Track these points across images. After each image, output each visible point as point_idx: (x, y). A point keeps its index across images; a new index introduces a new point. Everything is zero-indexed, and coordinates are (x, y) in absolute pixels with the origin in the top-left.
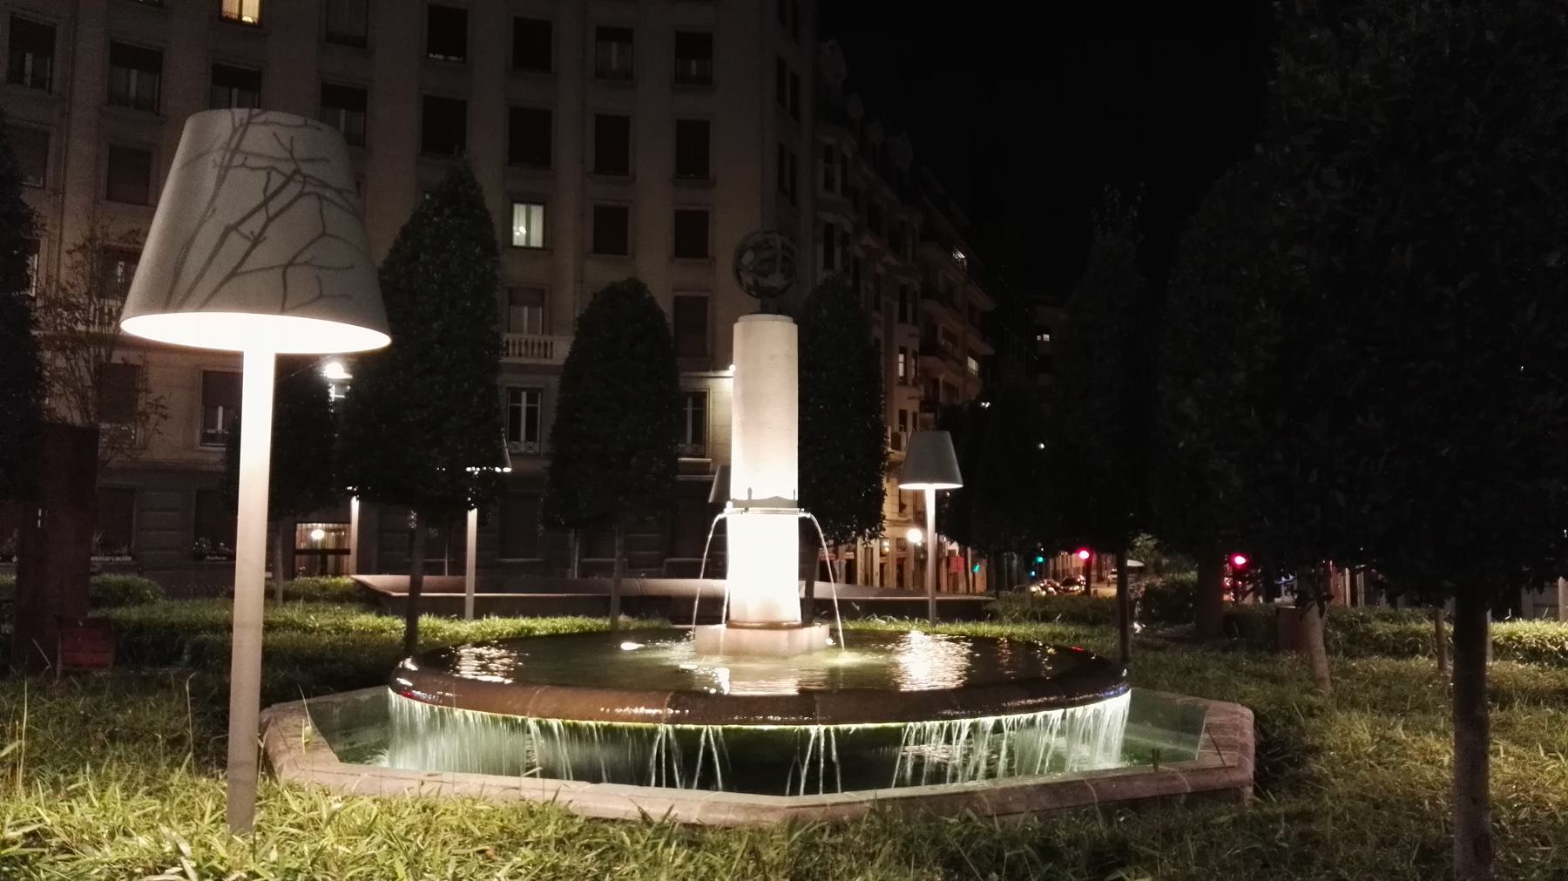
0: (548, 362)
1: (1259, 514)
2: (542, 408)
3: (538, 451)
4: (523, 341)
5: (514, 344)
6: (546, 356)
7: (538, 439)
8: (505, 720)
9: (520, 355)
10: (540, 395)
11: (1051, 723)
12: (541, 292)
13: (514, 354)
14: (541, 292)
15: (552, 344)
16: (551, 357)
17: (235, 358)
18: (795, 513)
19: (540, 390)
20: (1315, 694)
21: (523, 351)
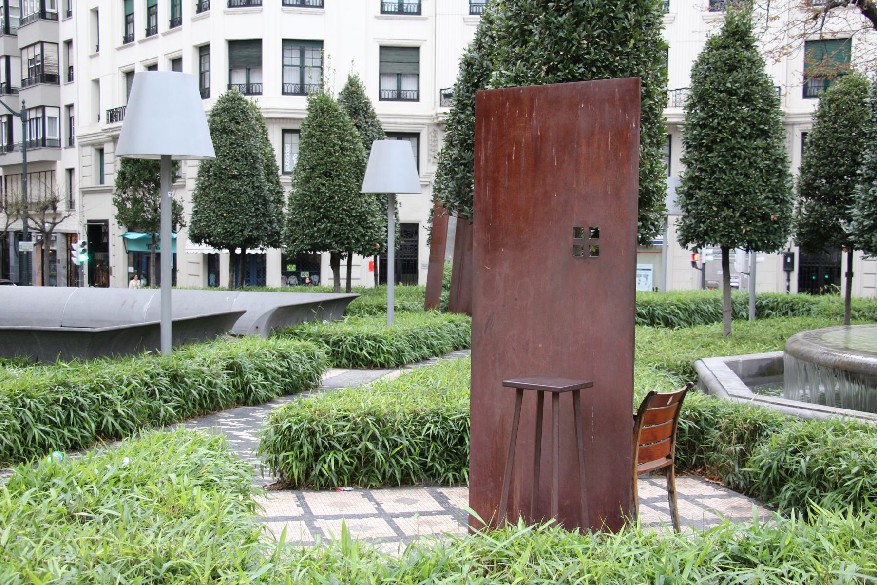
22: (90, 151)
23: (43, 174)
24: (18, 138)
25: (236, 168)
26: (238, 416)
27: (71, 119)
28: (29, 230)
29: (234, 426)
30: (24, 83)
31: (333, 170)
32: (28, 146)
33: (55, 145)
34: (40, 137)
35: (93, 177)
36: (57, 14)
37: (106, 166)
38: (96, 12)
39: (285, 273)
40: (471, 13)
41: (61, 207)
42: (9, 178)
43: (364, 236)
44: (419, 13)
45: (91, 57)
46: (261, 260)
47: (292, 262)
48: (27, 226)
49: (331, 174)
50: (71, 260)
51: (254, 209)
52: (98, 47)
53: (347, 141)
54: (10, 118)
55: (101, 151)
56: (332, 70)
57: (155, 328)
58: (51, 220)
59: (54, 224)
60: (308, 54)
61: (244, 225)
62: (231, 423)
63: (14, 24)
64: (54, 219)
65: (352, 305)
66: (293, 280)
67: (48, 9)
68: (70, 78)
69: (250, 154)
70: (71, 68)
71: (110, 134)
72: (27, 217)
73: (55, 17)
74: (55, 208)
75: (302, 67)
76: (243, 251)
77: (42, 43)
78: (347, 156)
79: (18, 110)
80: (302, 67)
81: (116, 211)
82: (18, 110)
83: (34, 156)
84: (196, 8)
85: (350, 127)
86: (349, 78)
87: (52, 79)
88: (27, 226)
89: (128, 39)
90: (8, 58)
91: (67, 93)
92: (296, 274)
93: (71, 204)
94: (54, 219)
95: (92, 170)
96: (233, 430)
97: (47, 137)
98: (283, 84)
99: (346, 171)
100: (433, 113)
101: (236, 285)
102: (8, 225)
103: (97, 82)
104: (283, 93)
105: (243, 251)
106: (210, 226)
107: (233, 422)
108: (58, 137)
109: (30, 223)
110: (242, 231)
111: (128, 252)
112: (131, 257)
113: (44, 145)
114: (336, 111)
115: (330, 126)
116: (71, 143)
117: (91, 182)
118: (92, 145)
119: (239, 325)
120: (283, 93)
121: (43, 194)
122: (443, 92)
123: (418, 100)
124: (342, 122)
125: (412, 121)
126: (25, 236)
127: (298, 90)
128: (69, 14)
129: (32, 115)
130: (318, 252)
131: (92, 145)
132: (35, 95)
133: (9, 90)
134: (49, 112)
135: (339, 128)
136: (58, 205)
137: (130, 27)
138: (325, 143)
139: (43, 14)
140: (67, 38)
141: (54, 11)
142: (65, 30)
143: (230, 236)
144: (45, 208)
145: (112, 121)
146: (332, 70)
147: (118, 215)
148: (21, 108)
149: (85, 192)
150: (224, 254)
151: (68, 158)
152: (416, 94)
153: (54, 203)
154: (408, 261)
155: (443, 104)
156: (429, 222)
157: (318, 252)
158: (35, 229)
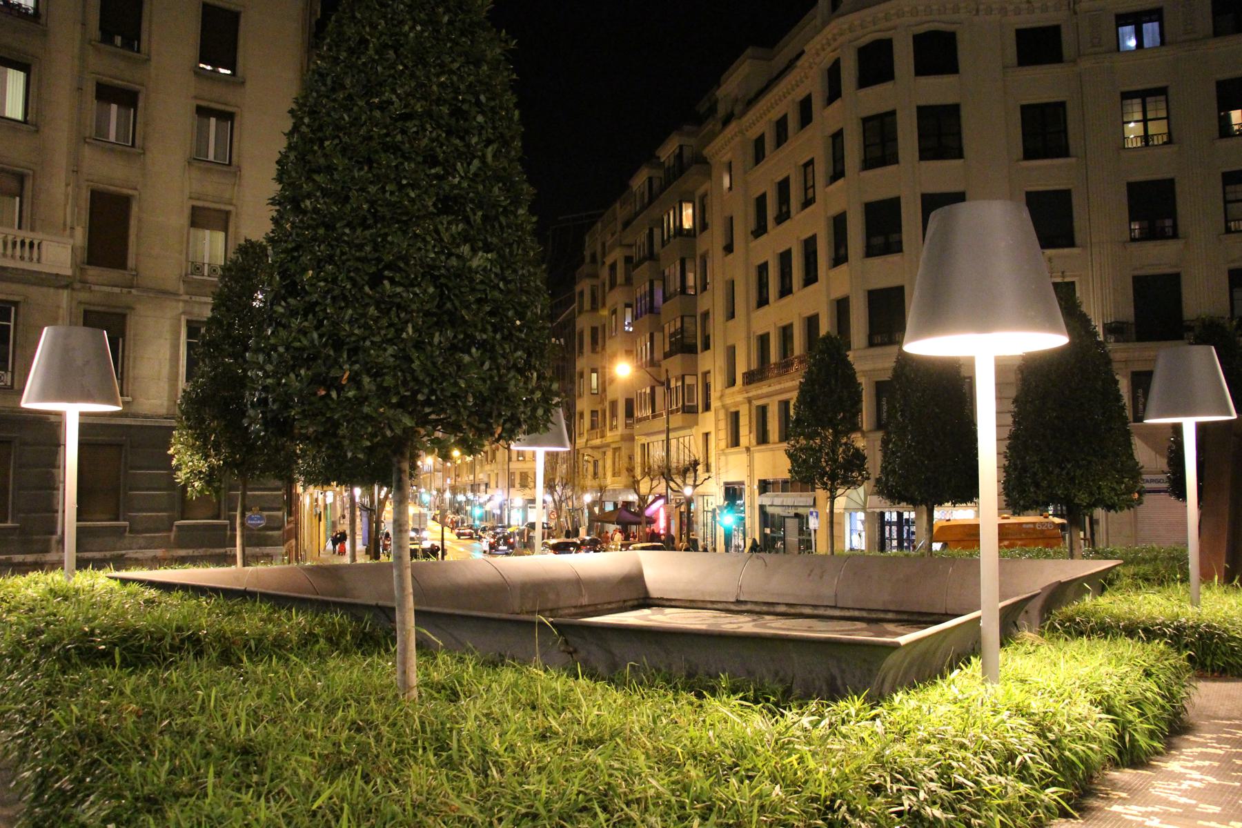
0: (35, 267)
1: (323, 393)
2: (15, 325)
3: (9, 384)
4: (27, 241)
5: (14, 244)
6: (31, 259)
7: (10, 369)
8: (704, 802)
9: (22, 258)
10: (13, 309)
11: (1074, 758)
12: (21, 178)
13: (13, 257)
14: (21, 178)
15: (39, 245)
16: (39, 260)
17: (970, 363)
18: (751, 475)
19: (16, 304)
20: (250, 659)
21: (27, 254)
42: (651, 445)
97: (686, 404)
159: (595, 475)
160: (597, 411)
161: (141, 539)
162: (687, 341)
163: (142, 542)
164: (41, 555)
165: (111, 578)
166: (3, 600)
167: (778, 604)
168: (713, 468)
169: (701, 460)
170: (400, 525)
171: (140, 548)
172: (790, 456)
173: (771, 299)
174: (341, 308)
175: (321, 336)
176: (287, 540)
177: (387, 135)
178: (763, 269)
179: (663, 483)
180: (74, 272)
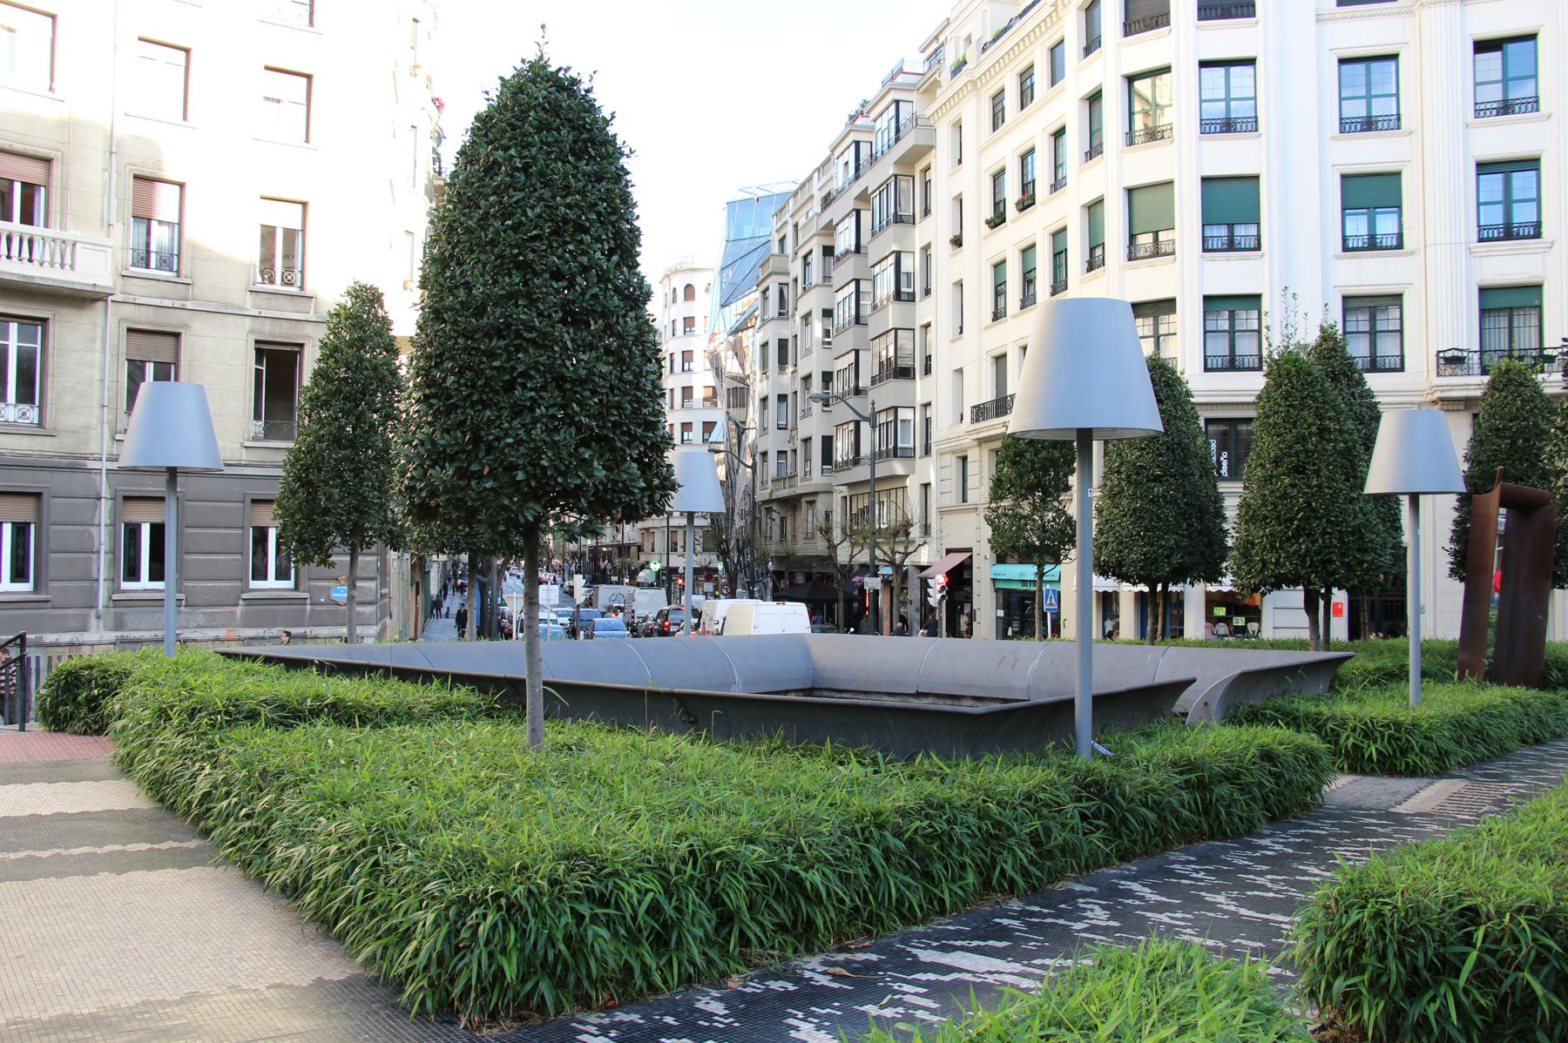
3: (36, 421)
16: (72, 267)
22: (952, 462)
23: (893, 492)
24: (865, 450)
25: (1158, 466)
26: (1203, 859)
27: (928, 421)
28: (877, 563)
29: (1202, 880)
30: (873, 382)
31: (1308, 463)
32: (876, 457)
33: (907, 455)
34: (891, 446)
35: (954, 493)
36: (913, 294)
37: (969, 479)
38: (960, 284)
39: (1211, 619)
40: (1481, 240)
41: (915, 532)
42: (854, 499)
43: (1361, 562)
44: (1400, 246)
45: (953, 341)
46: (1178, 602)
47: (1220, 605)
48: (873, 557)
49: (1305, 469)
50: (926, 601)
51: (1185, 526)
52: (961, 328)
53: (1330, 418)
54: (857, 424)
55: (964, 459)
56: (1300, 315)
57: (1065, 707)
58: (902, 550)
59: (907, 554)
60: (1241, 315)
61: (1171, 548)
62: (1194, 875)
63: (866, 310)
64: (906, 548)
65: (1343, 670)
66: (1222, 628)
67: (904, 289)
68: (928, 371)
69: (1179, 444)
70: (928, 358)
71: (976, 436)
72: (876, 545)
73: (911, 298)
74: (907, 534)
75: (1232, 332)
76: (1165, 587)
77: (896, 330)
78: (1330, 441)
79: (868, 413)
80: (1232, 332)
81: (988, 532)
82: (868, 413)
83: (881, 471)
84: (1086, 265)
85: (1333, 398)
86: (1322, 329)
87: (905, 373)
88: (873, 557)
89: (998, 315)
90: (858, 282)
91: (921, 388)
92: (1226, 620)
93: (926, 529)
94: (906, 548)
95: (953, 486)
96: (1202, 889)
97: (900, 445)
98: (1205, 357)
99: (1330, 464)
100: (1425, 386)
101: (1163, 635)
102: (852, 557)
103: (960, 371)
104: (1206, 369)
105: (1165, 587)
106: (1121, 551)
107: (1197, 871)
108: (911, 445)
109: (878, 552)
110: (1168, 557)
111: (997, 590)
112: (1001, 596)
113: (895, 456)
114: (1310, 375)
115: (1303, 399)
116: (927, 451)
117: (952, 499)
118: (953, 452)
119: (1188, 701)
120: (1206, 369)
121: (893, 517)
122: (1441, 355)
123: (1402, 369)
124: (1320, 391)
125: (1394, 399)
126: (872, 569)
127: (1226, 365)
128: (927, 292)
129: (882, 418)
130: (1172, 588)
131: (953, 452)
132: (889, 393)
133: (858, 391)
134: (904, 414)
135: (1315, 399)
136: (911, 530)
137: (1095, 136)
138: (1295, 424)
139: (898, 296)
140: (925, 322)
141: (911, 290)
142: (924, 311)
143: (1152, 564)
144: (896, 534)
145: (977, 420)
146: (1300, 315)
147: (1375, 407)
148: (870, 411)
149: (943, 512)
150: (1127, 592)
151: (928, 470)
152: (1398, 359)
153: (907, 525)
154: (1392, 602)
155: (1441, 372)
156: (1452, 540)
157: (1172, 588)
158: (884, 561)
159: (783, 535)
160: (785, 452)
161: (200, 615)
162: (902, 363)
163: (201, 619)
164: (77, 634)
165: (228, 655)
166: (1566, 457)
167: (965, 697)
168: (933, 531)
169: (916, 520)
170: (531, 604)
171: (199, 627)
172: (990, 521)
173: (1010, 312)
174: (479, 411)
175: (464, 434)
176: (381, 618)
177: (519, 254)
178: (999, 266)
179: (866, 551)
180: (115, 283)
